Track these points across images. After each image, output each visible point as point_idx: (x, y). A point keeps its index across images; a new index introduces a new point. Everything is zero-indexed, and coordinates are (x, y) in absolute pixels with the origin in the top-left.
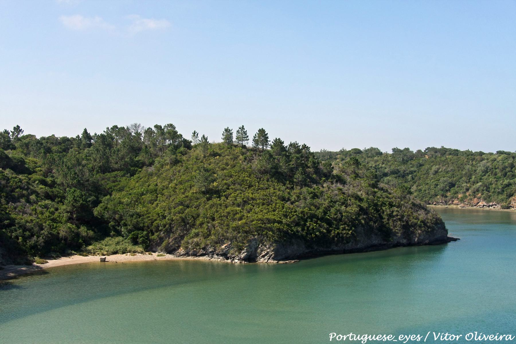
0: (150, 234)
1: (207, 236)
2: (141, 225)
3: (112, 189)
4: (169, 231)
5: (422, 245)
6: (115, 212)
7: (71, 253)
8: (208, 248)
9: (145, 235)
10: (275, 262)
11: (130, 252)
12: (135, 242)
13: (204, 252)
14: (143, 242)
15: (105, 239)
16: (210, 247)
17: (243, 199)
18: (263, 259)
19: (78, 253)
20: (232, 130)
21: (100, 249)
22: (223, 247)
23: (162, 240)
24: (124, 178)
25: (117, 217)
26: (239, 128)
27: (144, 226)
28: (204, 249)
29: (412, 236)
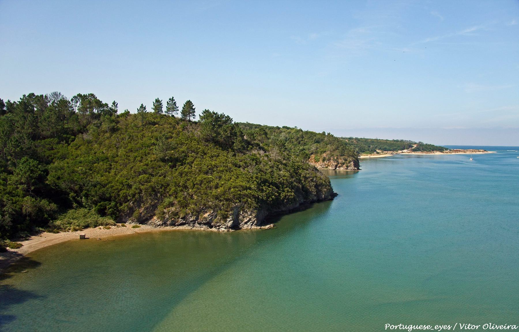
0: (118, 205)
1: (184, 205)
2: (108, 195)
3: (53, 157)
4: (139, 202)
5: (327, 200)
6: (73, 182)
7: (39, 230)
8: (188, 218)
9: (114, 206)
10: (259, 228)
11: (102, 225)
12: (102, 212)
13: (184, 221)
14: (112, 214)
15: (69, 212)
16: (190, 216)
17: (208, 166)
18: (245, 226)
19: (47, 230)
20: (162, 101)
21: (68, 223)
22: (206, 215)
23: (132, 210)
24: (60, 145)
25: (77, 187)
26: (170, 99)
27: (111, 197)
28: (183, 218)
29: (320, 194)
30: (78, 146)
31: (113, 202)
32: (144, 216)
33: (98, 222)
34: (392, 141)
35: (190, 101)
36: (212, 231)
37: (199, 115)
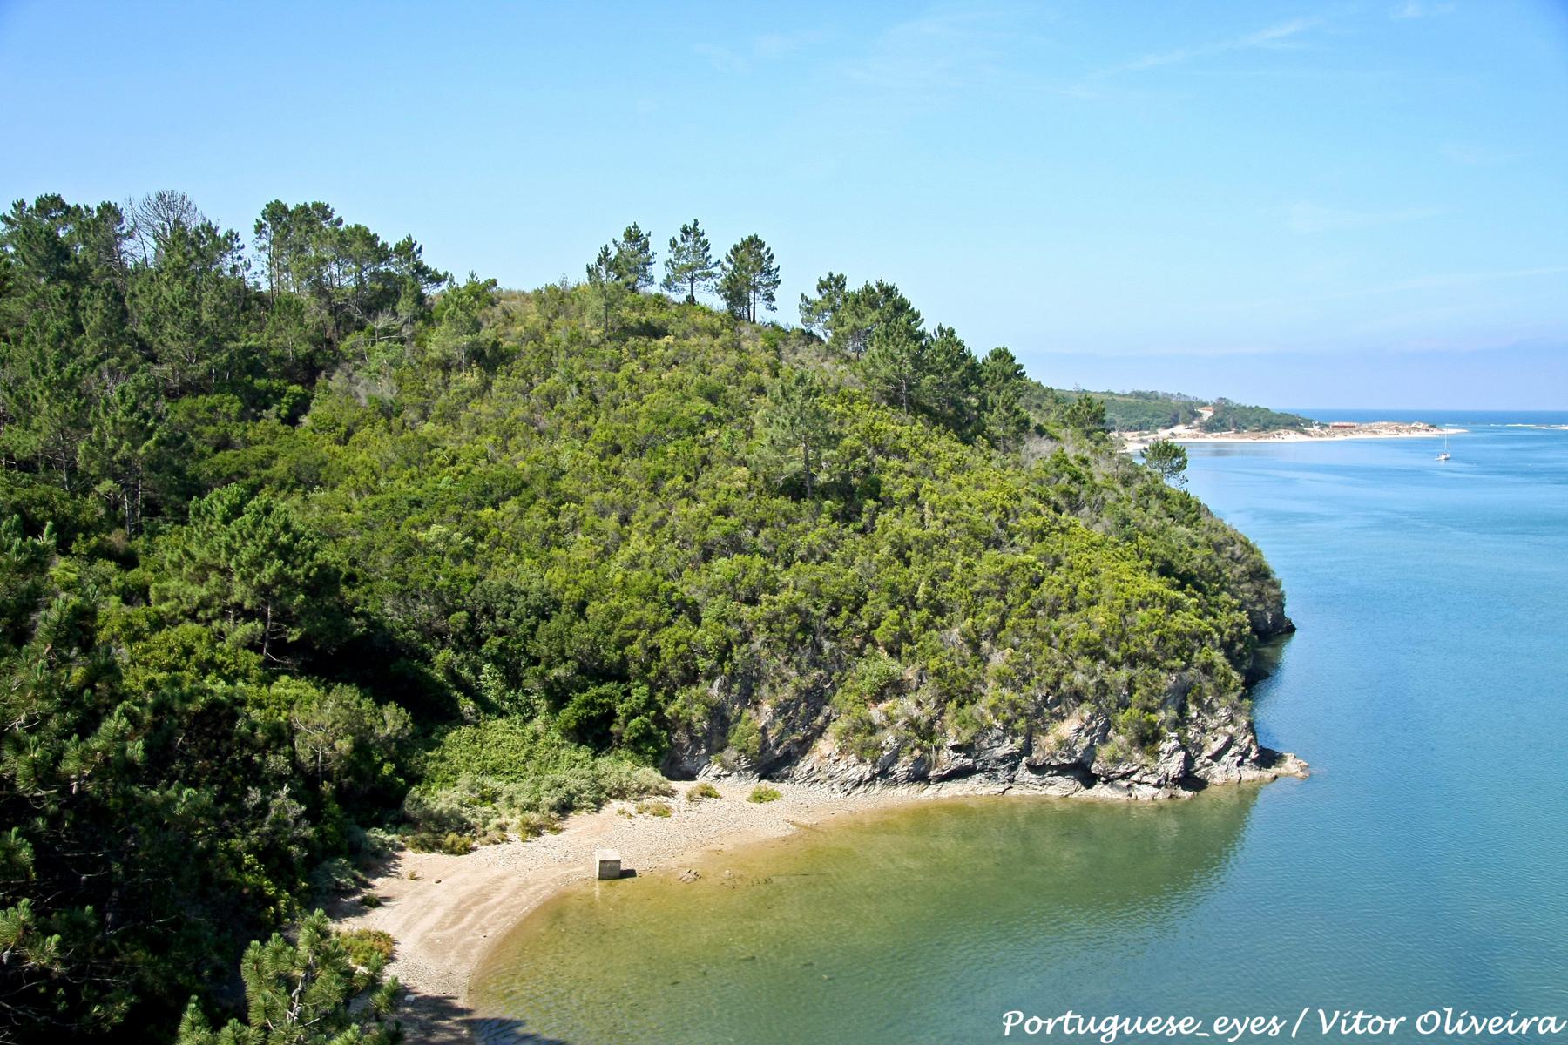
4: (748, 686)
8: (985, 744)
13: (970, 762)
22: (1067, 729)
27: (624, 661)
30: (343, 429)
31: (638, 687)
32: (777, 745)
33: (602, 782)
34: (1131, 395)
35: (756, 236)
36: (1091, 806)
37: (802, 295)
